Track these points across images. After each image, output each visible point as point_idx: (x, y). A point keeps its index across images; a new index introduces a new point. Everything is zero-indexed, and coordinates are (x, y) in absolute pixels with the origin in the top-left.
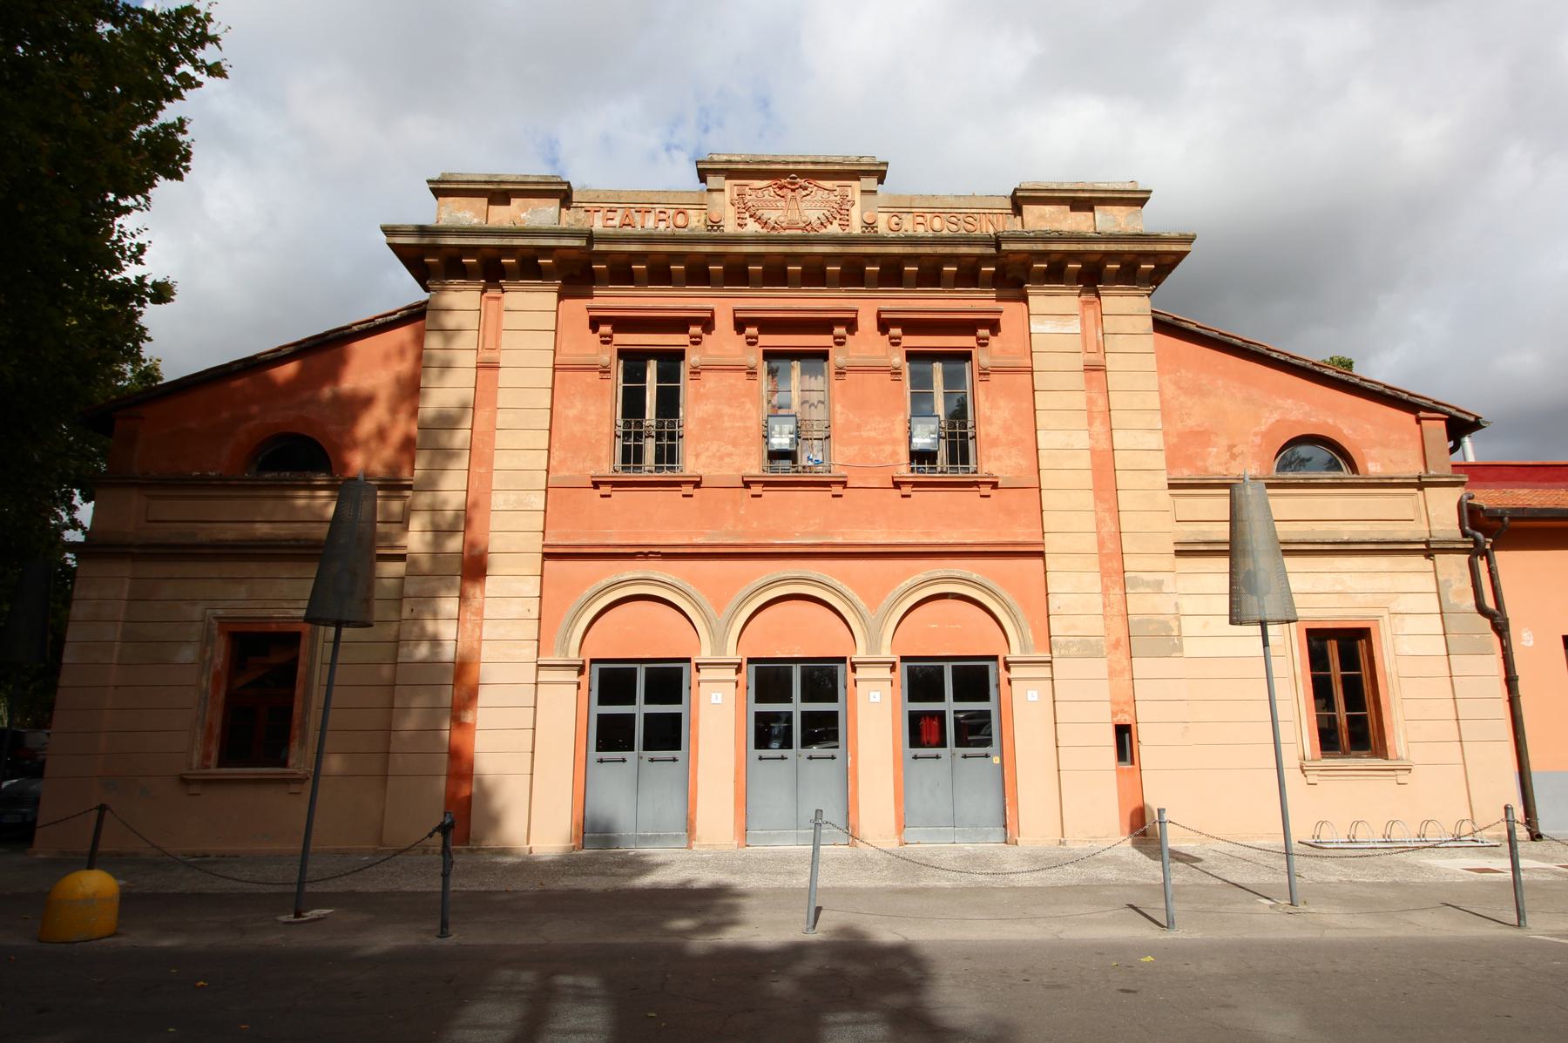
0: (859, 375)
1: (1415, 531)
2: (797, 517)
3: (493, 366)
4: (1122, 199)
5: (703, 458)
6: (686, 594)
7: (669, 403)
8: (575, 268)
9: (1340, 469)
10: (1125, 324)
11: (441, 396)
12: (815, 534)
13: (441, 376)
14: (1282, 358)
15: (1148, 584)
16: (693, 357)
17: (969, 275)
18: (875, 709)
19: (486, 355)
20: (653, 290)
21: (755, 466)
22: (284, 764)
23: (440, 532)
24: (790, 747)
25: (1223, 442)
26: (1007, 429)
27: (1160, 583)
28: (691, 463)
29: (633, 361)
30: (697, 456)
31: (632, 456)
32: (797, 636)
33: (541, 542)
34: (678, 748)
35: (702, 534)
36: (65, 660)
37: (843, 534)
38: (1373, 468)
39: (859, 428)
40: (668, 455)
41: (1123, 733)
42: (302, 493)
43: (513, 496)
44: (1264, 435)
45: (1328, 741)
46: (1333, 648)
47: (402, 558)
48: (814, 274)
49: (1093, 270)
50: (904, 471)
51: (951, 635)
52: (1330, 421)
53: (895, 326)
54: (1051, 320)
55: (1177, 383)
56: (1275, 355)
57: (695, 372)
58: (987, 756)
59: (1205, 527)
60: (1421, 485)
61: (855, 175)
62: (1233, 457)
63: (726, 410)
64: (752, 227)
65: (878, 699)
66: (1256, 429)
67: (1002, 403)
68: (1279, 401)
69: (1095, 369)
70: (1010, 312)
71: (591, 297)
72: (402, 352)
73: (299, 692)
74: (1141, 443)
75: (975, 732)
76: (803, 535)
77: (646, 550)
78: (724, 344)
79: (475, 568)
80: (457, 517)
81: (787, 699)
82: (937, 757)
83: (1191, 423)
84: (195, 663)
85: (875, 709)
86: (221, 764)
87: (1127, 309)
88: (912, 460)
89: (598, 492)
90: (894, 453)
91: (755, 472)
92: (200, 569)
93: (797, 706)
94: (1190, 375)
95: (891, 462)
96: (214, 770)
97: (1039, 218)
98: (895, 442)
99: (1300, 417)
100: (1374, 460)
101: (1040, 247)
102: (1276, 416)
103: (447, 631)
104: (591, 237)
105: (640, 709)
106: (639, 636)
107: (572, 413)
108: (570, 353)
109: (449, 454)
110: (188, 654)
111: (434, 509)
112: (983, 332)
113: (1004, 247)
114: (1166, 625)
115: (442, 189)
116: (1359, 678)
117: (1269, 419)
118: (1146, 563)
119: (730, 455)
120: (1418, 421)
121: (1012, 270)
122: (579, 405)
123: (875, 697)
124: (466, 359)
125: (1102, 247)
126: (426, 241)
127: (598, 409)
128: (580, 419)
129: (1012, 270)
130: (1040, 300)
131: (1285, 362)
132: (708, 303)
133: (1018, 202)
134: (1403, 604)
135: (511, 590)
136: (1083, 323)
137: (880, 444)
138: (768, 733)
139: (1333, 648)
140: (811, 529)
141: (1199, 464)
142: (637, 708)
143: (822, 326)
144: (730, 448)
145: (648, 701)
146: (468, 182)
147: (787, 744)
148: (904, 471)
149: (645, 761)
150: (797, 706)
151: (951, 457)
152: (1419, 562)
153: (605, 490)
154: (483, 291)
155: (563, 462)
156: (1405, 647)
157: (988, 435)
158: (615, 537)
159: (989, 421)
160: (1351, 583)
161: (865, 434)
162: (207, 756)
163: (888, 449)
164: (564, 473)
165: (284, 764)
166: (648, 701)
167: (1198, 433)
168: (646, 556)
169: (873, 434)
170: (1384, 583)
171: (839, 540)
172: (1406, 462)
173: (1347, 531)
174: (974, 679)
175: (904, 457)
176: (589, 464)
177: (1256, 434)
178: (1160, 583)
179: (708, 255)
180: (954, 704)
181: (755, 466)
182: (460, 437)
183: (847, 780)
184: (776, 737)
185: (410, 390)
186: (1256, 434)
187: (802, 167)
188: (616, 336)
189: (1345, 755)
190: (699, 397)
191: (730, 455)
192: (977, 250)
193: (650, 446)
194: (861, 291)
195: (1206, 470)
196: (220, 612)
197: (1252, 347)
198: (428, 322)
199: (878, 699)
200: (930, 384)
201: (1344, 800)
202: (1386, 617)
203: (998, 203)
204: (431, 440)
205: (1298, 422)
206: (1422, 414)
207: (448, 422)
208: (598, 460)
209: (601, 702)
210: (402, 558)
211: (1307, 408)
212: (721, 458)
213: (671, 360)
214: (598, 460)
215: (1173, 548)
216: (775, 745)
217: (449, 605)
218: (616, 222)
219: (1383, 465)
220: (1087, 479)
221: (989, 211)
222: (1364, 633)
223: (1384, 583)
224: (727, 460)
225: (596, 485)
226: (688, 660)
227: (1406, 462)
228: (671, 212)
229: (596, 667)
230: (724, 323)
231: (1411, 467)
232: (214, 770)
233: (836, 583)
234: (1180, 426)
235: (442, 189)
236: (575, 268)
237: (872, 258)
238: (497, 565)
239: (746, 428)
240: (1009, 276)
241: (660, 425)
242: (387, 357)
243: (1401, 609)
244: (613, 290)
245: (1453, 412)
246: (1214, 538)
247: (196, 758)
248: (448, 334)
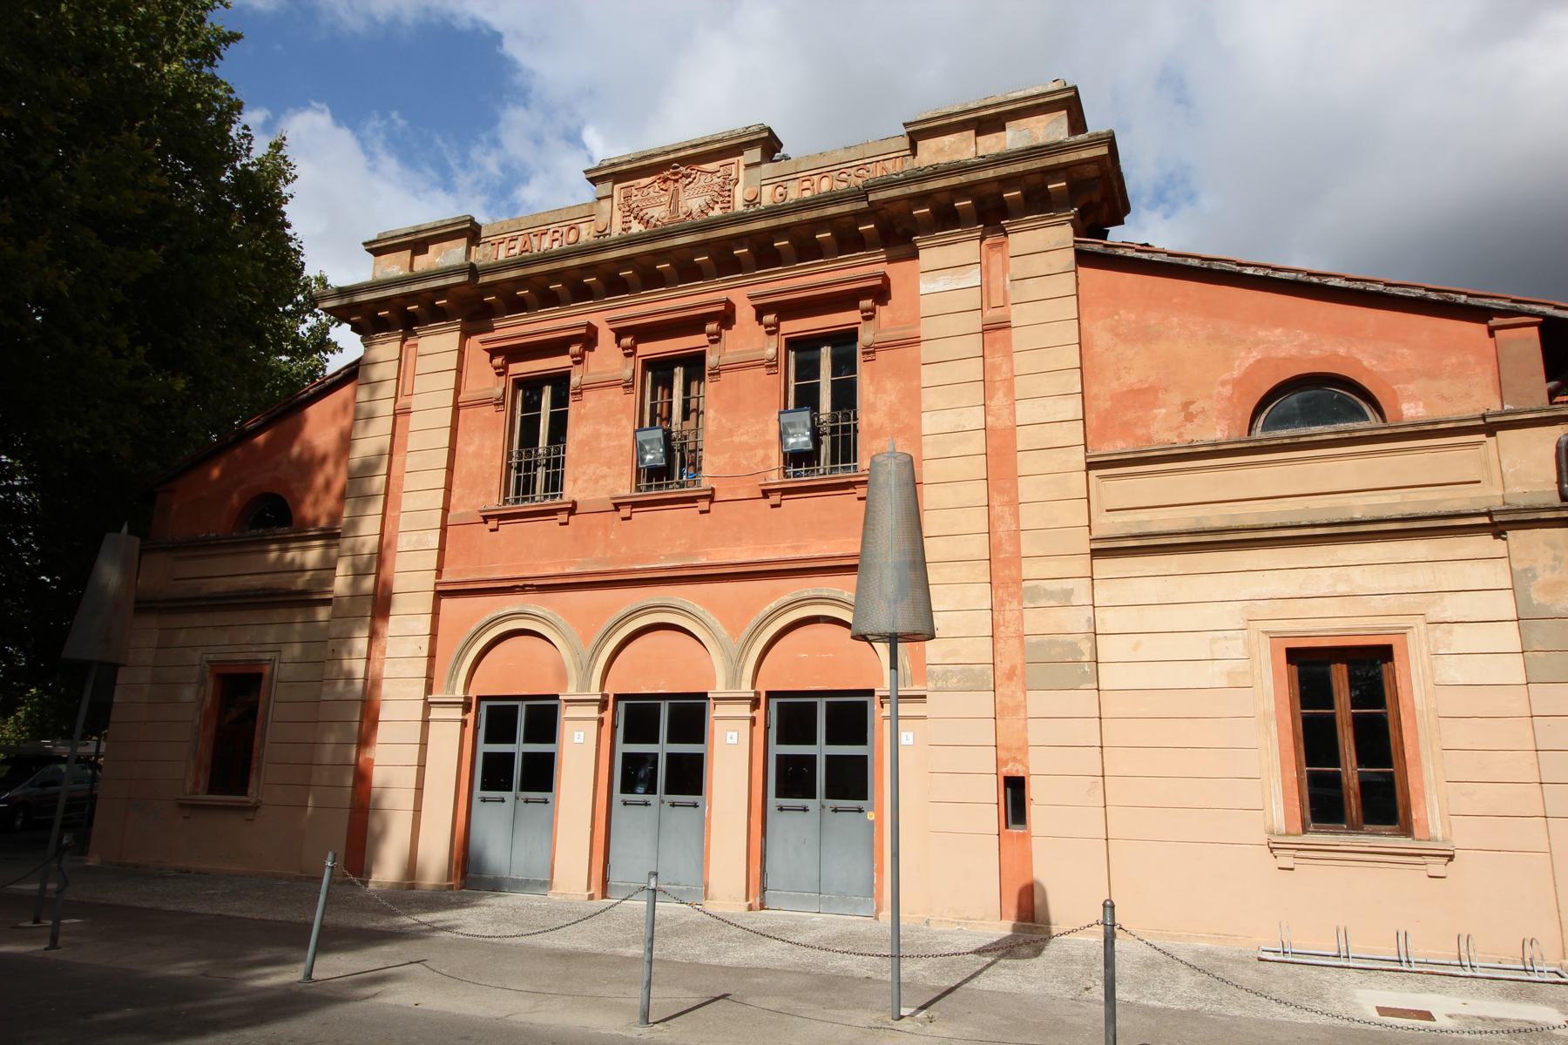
0: (734, 374)
1: (1488, 496)
2: (668, 536)
3: (407, 412)
4: (1039, 105)
5: (580, 484)
6: (705, 626)
7: (845, 396)
8: (471, 304)
9: (1364, 417)
10: (1038, 264)
11: (367, 445)
12: (680, 556)
13: (367, 425)
14: (1261, 273)
15: (1051, 595)
16: (866, 336)
17: (848, 240)
18: (733, 750)
19: (991, 314)
20: (544, 313)
21: (624, 487)
22: (245, 794)
23: (358, 574)
24: (814, 797)
25: (1176, 398)
26: (893, 415)
27: (1068, 593)
28: (571, 491)
29: (804, 346)
30: (575, 481)
31: (526, 487)
32: (655, 670)
33: (1087, 537)
34: (865, 798)
35: (572, 563)
36: (115, 700)
37: (707, 554)
38: (1412, 411)
39: (731, 433)
40: (554, 484)
41: (1015, 789)
42: (274, 547)
43: (414, 537)
44: (1237, 383)
45: (1324, 805)
46: (1339, 675)
47: (328, 602)
48: (686, 269)
49: (987, 206)
50: (775, 478)
51: (821, 664)
52: (1342, 351)
53: (769, 313)
54: (942, 278)
55: (1114, 331)
56: (1249, 271)
57: (870, 351)
58: (860, 811)
59: (1144, 515)
60: (1490, 429)
61: (736, 150)
62: (1189, 417)
63: (604, 429)
64: (636, 228)
65: (735, 735)
66: (1226, 376)
67: (889, 385)
68: (1262, 334)
69: (996, 328)
70: (897, 272)
71: (492, 330)
72: (345, 407)
73: (258, 727)
74: (1048, 412)
75: (850, 781)
76: (668, 557)
77: (521, 583)
78: (608, 360)
79: (381, 604)
80: (370, 560)
81: (812, 740)
82: (805, 810)
83: (1131, 379)
84: (194, 697)
85: (733, 750)
86: (210, 792)
87: (1045, 243)
88: (786, 464)
89: (766, 503)
90: (767, 458)
91: (627, 492)
92: (198, 619)
93: (660, 746)
94: (1133, 316)
95: (762, 469)
96: (203, 797)
97: (933, 152)
98: (767, 445)
99: (1294, 352)
100: (1412, 398)
101: (914, 189)
102: (1256, 355)
103: (359, 667)
104: (473, 271)
105: (663, 748)
106: (512, 673)
107: (471, 449)
108: (470, 391)
109: (367, 498)
110: (188, 694)
111: (355, 553)
112: (866, 303)
113: (872, 197)
114: (1074, 648)
115: (378, 248)
116: (1331, 720)
117: (1244, 360)
118: (1053, 568)
119: (604, 477)
120: (1491, 333)
121: (894, 221)
122: (477, 440)
123: (732, 738)
124: (385, 408)
125: (991, 173)
126: (346, 301)
127: (488, 445)
128: (478, 455)
129: (894, 221)
130: (931, 255)
131: (1266, 278)
132: (723, 295)
133: (917, 134)
134: (1451, 608)
135: (407, 628)
136: (985, 272)
137: (752, 448)
138: (793, 780)
139: (1339, 675)
140: (677, 550)
141: (1140, 432)
142: (512, 747)
143: (845, 301)
144: (605, 470)
145: (830, 741)
146: (393, 238)
147: (651, 789)
148: (775, 478)
149: (666, 805)
150: (660, 746)
151: (826, 453)
152: (1484, 544)
153: (493, 524)
154: (982, 239)
155: (461, 499)
156: (1453, 671)
157: (870, 425)
158: (499, 571)
159: (872, 408)
160: (1362, 580)
161: (736, 439)
162: (196, 784)
163: (760, 453)
164: (461, 510)
165: (245, 794)
166: (830, 741)
167: (1140, 391)
168: (523, 589)
169: (745, 438)
170: (1422, 578)
171: (703, 561)
172: (1468, 395)
173: (1359, 507)
174: (850, 716)
175: (776, 459)
176: (482, 499)
177: (1223, 384)
178: (1068, 593)
179: (581, 267)
180: (825, 750)
181: (624, 487)
182: (378, 482)
183: (703, 827)
184: (642, 781)
185: (346, 442)
186: (1223, 384)
187: (682, 154)
188: (511, 366)
189: (1355, 828)
190: (580, 417)
191: (604, 477)
192: (846, 208)
193: (541, 473)
194: (738, 279)
195: (1149, 440)
196: (211, 657)
197: (1216, 266)
198: (360, 379)
199: (735, 735)
200: (816, 373)
201: (1352, 893)
202: (1422, 627)
203: (893, 145)
204: (356, 489)
205: (1290, 359)
206: (1496, 321)
207: (368, 468)
208: (490, 494)
209: (488, 740)
210: (328, 602)
211: (1306, 337)
212: (596, 481)
213: (844, 340)
214: (490, 494)
215: (1086, 548)
216: (640, 789)
217: (361, 643)
218: (517, 251)
219: (1426, 405)
220: (978, 467)
221: (885, 157)
222: (1384, 653)
223: (1422, 578)
224: (602, 482)
225: (486, 519)
226: (871, 693)
227: (1468, 395)
228: (565, 229)
229: (774, 702)
230: (745, 312)
231: (1481, 400)
232: (203, 797)
233: (698, 609)
234: (1115, 385)
235: (378, 248)
236: (471, 304)
237: (738, 240)
238: (400, 605)
239: (621, 447)
240: (899, 230)
241: (834, 419)
242: (335, 414)
243: (1447, 616)
244: (510, 320)
245: (1549, 311)
246: (1155, 529)
247: (189, 785)
248: (374, 385)
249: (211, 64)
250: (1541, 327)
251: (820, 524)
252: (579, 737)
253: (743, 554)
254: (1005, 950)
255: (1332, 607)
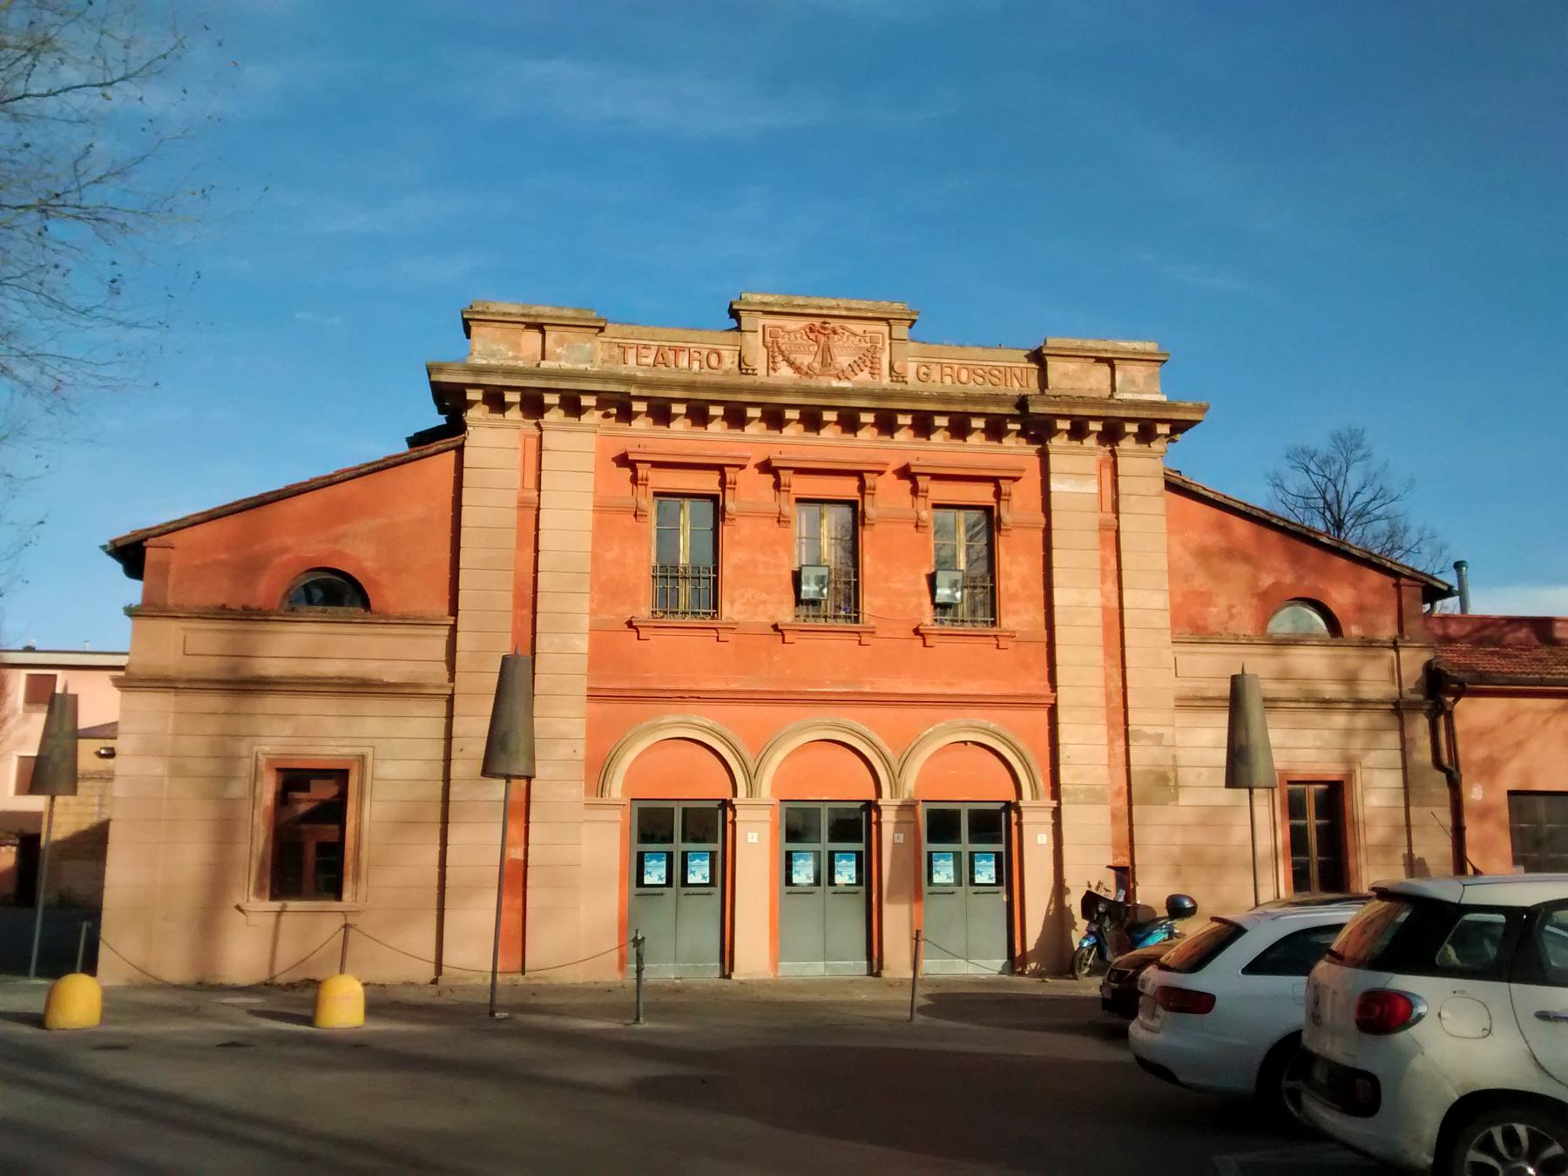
5: (738, 605)
12: (844, 683)
15: (1149, 737)
30: (732, 603)
63: (760, 557)
67: (1021, 558)
119: (764, 603)
144: (764, 596)
161: (893, 586)
163: (914, 600)
169: (899, 586)
171: (867, 689)
191: (764, 603)
199: (755, 840)
249: (1020, 434)
250: (1424, 589)
251: (961, 663)
252: (753, 837)
253: (905, 686)
254: (1410, 855)
255: (285, 662)
